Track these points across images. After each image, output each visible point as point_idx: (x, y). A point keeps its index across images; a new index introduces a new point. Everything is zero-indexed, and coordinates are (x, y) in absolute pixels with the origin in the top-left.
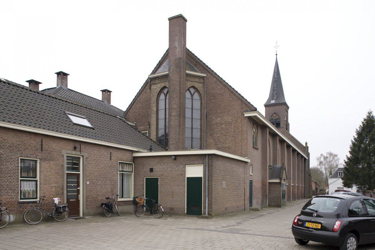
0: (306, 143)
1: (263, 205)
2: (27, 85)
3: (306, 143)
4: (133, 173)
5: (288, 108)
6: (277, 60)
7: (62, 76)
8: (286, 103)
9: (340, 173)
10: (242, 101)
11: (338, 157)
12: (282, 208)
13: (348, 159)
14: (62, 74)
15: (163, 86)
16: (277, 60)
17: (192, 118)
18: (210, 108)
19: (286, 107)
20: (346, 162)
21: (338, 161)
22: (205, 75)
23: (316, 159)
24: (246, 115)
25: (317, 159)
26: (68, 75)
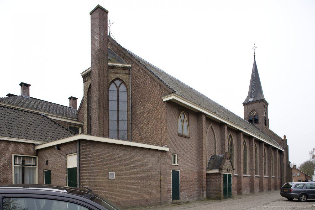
0: (285, 136)
1: (200, 198)
2: (6, 97)
3: (285, 136)
4: (37, 167)
5: (267, 104)
6: (255, 60)
7: (25, 87)
12: (222, 201)
14: (23, 85)
16: (255, 60)
17: (118, 111)
18: (135, 98)
19: (264, 103)
22: (131, 66)
23: (309, 153)
24: (164, 100)
25: (310, 153)
26: (30, 85)
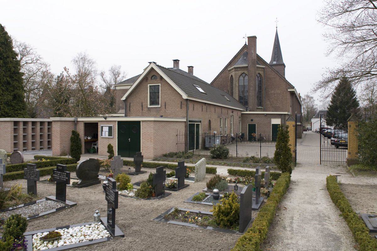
5: (285, 66)
6: (277, 31)
8: (284, 64)
9: (321, 114)
10: (286, 83)
11: (314, 99)
13: (330, 106)
15: (242, 73)
16: (277, 31)
20: (328, 109)
21: (314, 102)
22: (264, 67)
24: (289, 90)
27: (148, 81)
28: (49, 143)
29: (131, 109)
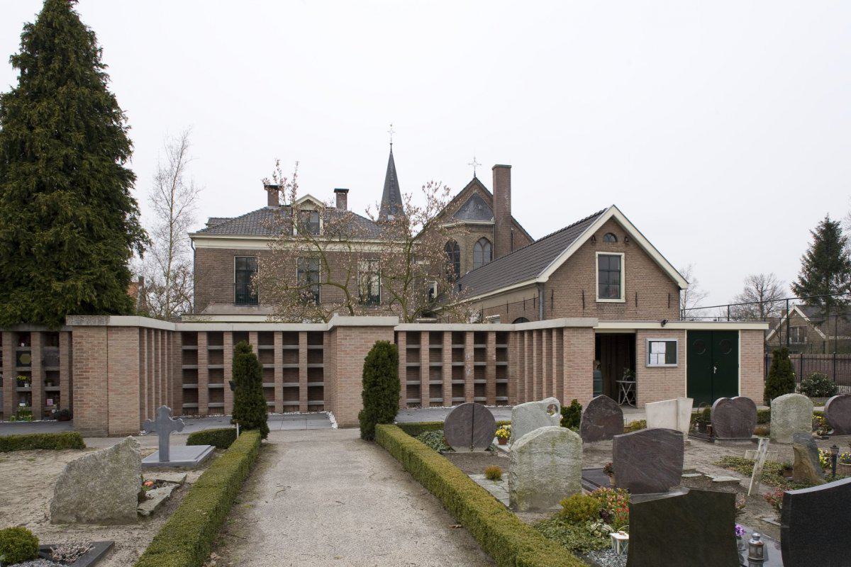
6: (391, 152)
16: (391, 152)
27: (597, 244)
28: (316, 392)
29: (555, 303)
